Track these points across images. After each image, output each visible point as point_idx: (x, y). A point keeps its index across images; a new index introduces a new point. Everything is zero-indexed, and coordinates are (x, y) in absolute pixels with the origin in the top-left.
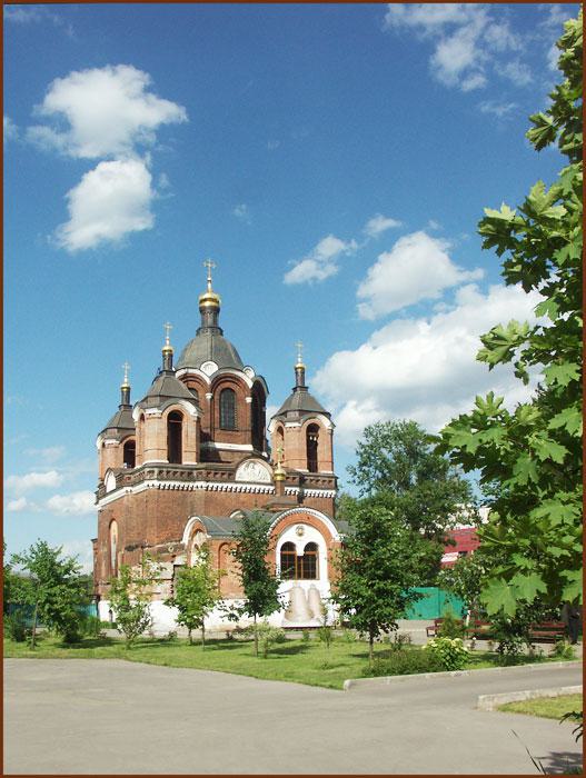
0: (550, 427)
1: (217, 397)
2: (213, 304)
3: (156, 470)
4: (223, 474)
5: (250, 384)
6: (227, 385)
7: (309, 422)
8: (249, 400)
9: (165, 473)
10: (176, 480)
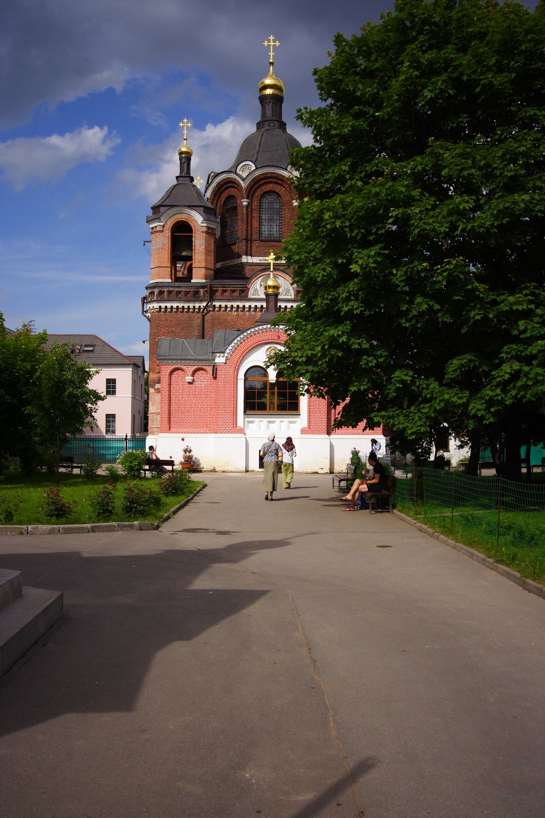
1: (255, 203)
2: (276, 92)
3: (156, 291)
4: (234, 291)
6: (269, 187)
9: (166, 294)
10: (180, 300)
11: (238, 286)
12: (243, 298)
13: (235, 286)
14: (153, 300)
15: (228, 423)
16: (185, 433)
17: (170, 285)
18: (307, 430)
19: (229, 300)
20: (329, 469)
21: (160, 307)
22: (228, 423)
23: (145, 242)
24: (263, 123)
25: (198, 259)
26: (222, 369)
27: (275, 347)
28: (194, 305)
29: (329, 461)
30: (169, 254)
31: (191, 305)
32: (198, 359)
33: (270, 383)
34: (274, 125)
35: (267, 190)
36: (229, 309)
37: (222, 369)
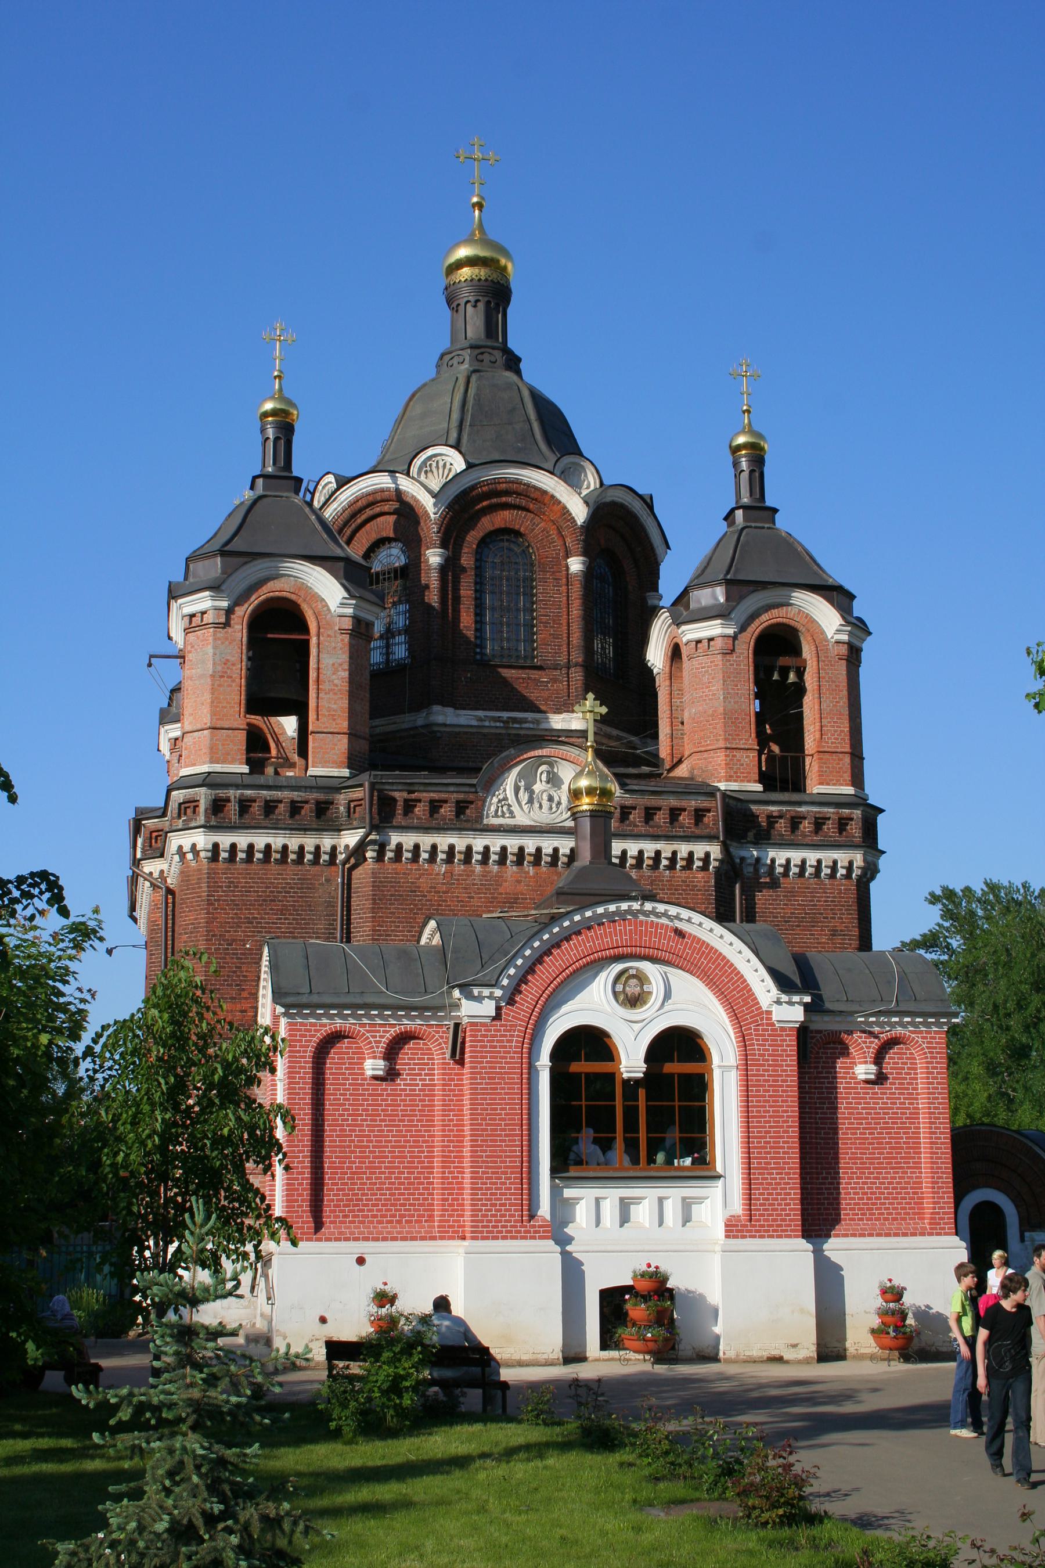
0: (377, 635)
1: (467, 560)
3: (203, 796)
5: (580, 513)
7: (766, 620)
8: (576, 565)
11: (452, 789)
12: (469, 825)
13: (444, 789)
14: (193, 824)
15: (505, 1205)
16: (366, 1239)
17: (248, 780)
18: (742, 1226)
19: (426, 829)
20: (814, 1348)
21: (216, 846)
22: (505, 1205)
23: (151, 656)
24: (460, 352)
25: (329, 709)
26: (486, 1036)
27: (637, 969)
28: (317, 841)
29: (813, 1322)
30: (243, 693)
31: (310, 842)
32: (402, 1003)
33: (626, 1082)
34: (493, 359)
35: (497, 526)
36: (665, 862)
37: (486, 1036)
